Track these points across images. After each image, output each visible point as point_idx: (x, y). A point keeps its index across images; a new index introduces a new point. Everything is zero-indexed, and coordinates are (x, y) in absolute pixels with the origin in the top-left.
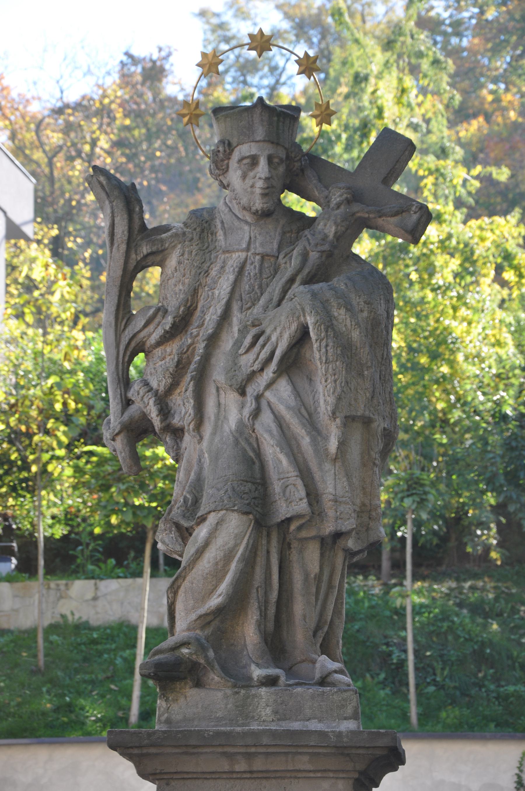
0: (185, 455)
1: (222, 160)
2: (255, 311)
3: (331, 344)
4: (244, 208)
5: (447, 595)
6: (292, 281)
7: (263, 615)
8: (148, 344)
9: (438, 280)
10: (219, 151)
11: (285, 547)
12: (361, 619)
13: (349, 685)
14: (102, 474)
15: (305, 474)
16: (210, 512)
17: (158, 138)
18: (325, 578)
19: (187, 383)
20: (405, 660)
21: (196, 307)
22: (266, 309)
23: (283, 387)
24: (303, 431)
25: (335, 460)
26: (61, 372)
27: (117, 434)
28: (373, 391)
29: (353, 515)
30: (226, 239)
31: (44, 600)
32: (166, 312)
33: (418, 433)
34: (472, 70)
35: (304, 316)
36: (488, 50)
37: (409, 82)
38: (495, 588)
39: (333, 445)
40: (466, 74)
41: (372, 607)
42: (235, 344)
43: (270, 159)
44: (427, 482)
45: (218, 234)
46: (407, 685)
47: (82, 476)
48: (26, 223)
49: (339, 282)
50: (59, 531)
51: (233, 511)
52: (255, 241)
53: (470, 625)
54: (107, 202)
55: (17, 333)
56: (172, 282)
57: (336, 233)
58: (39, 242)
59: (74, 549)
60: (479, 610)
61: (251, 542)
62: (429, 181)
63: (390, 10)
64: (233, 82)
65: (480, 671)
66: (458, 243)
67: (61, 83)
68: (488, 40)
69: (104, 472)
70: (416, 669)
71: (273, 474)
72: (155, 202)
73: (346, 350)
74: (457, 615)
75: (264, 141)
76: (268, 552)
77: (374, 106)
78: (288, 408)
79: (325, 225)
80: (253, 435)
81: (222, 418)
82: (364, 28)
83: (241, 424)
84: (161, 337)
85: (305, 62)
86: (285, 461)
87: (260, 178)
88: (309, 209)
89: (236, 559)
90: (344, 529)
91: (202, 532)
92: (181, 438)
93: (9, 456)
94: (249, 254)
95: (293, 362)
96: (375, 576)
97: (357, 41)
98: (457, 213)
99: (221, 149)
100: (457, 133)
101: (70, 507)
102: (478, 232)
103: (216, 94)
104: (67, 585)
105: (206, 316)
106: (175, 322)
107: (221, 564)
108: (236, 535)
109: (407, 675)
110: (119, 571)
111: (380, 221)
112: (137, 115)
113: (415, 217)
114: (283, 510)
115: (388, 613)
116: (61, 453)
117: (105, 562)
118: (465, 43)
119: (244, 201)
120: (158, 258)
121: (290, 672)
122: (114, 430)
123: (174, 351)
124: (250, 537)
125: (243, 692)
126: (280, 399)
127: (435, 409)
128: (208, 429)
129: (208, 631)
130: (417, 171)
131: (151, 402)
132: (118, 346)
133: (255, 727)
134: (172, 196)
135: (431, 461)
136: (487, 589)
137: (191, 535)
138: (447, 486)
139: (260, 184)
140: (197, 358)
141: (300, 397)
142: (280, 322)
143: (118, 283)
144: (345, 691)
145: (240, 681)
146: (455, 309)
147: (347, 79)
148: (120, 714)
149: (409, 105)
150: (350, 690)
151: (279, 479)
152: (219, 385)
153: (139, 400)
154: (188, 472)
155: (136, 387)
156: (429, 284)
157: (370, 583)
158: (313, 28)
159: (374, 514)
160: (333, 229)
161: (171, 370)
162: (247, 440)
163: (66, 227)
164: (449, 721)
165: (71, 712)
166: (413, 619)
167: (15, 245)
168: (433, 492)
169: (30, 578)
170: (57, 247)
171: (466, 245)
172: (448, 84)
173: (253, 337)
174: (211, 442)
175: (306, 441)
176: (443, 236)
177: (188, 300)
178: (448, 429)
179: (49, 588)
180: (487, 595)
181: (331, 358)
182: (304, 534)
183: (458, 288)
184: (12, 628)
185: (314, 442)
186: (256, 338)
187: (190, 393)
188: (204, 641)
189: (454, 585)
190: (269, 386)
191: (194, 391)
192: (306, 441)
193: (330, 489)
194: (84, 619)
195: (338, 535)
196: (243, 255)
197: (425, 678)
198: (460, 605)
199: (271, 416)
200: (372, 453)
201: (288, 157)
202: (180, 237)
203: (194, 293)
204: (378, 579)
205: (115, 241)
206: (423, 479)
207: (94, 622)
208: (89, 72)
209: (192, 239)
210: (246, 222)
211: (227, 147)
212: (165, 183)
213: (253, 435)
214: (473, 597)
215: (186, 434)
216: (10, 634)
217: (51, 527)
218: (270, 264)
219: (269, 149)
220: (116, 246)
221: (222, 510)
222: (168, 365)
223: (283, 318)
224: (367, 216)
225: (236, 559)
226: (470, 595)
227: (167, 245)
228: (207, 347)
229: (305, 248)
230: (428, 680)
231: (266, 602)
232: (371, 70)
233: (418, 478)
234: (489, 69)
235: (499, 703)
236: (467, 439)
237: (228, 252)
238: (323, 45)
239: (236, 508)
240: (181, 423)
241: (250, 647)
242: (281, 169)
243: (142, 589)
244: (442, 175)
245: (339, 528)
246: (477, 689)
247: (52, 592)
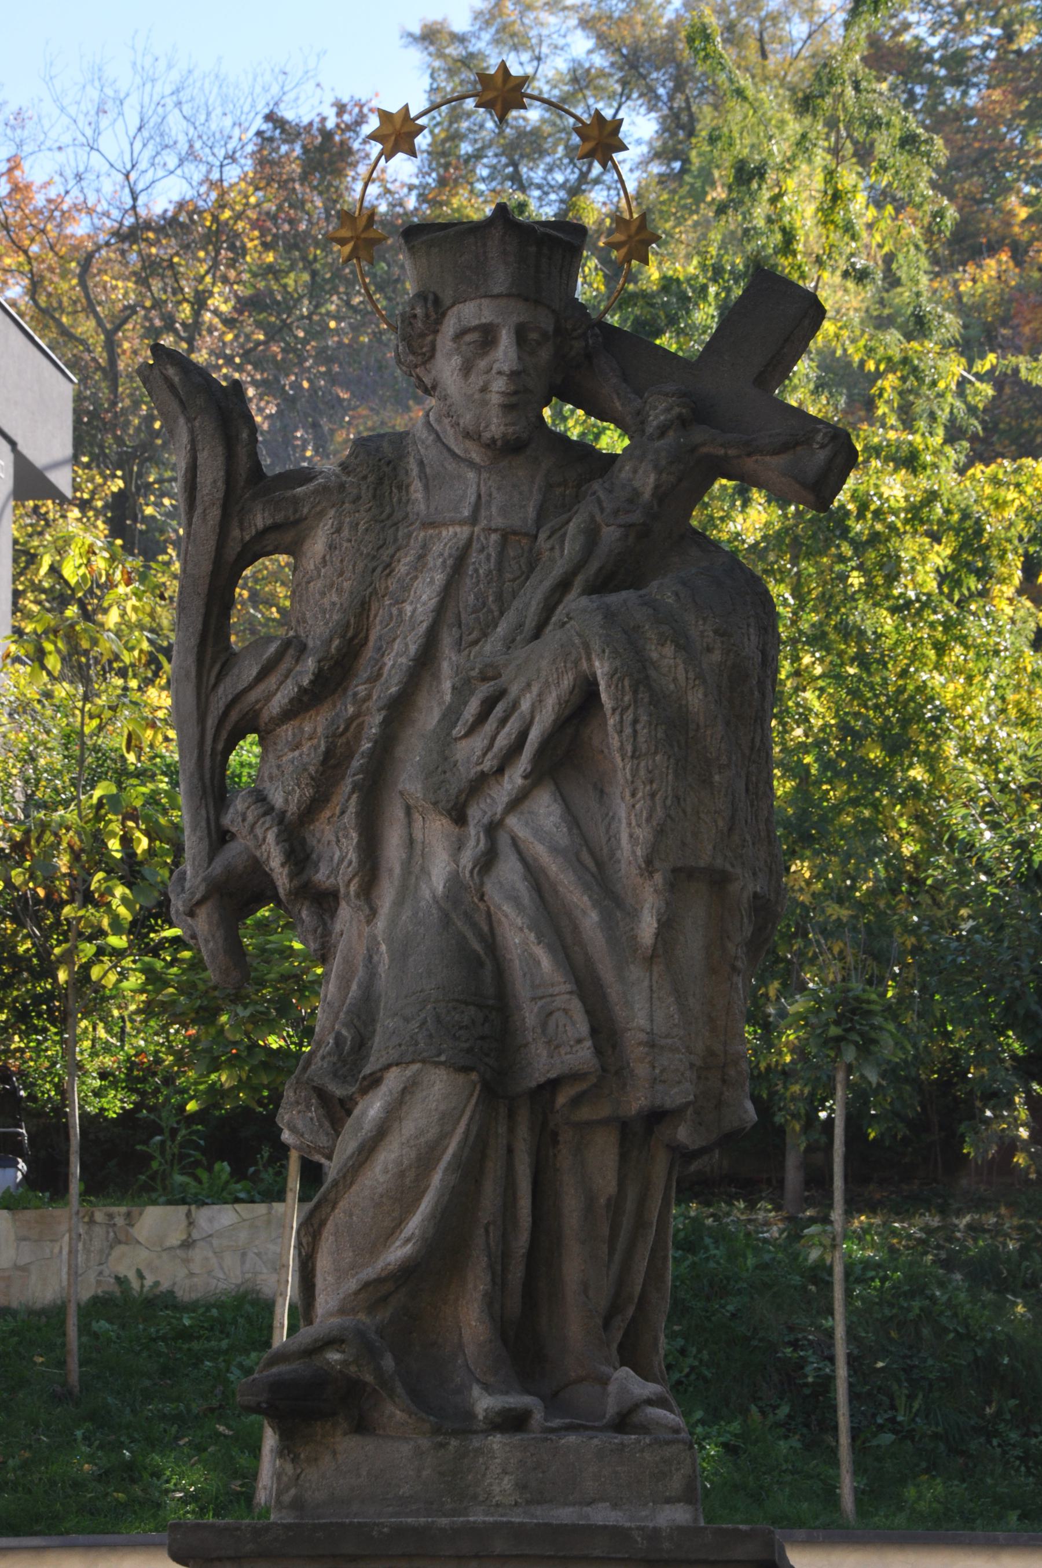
0: (340, 947)
1: (422, 335)
2: (488, 648)
3: (644, 718)
4: (467, 435)
5: (921, 1242)
6: (563, 586)
8: (265, 716)
9: (905, 588)
10: (415, 316)
11: (545, 1140)
12: (739, 1292)
13: (677, 1431)
14: (202, 987)
15: (588, 988)
16: (388, 1067)
17: (334, 290)
18: (630, 1205)
19: (345, 799)
20: (831, 1378)
21: (366, 638)
22: (510, 643)
23: (546, 808)
24: (585, 898)
25: (650, 960)
26: (122, 775)
27: (199, 903)
28: (733, 817)
29: (688, 1074)
30: (427, 499)
31: (80, 1246)
32: (303, 648)
33: (861, 907)
34: (986, 154)
35: (589, 659)
36: (1021, 115)
37: (848, 177)
38: (1022, 1229)
39: (647, 927)
40: (975, 163)
41: (764, 1267)
42: (444, 717)
43: (521, 335)
44: (877, 1008)
45: (412, 488)
46: (835, 1428)
47: (158, 992)
48: (56, 465)
49: (664, 590)
50: (115, 1104)
52: (489, 503)
53: (968, 1306)
54: (182, 421)
55: (32, 693)
56: (316, 586)
57: (657, 487)
58: (84, 505)
59: (146, 1142)
60: (990, 1275)
61: (474, 1129)
62: (890, 382)
63: (817, 31)
64: (491, 178)
65: (989, 1403)
66: (948, 512)
67: (133, 176)
68: (1021, 94)
69: (205, 981)
70: (854, 1396)
71: (521, 989)
72: (325, 424)
73: (675, 730)
74: (942, 1285)
75: (509, 296)
76: (510, 1151)
77: (776, 228)
79: (635, 472)
80: (481, 905)
81: (416, 869)
82: (764, 67)
83: (454, 881)
84: (291, 701)
85: (595, 133)
86: (546, 963)
87: (499, 373)
88: (612, 441)
89: (443, 1164)
90: (669, 1104)
91: (372, 1108)
92: (333, 913)
93: (15, 947)
95: (564, 755)
96: (771, 1201)
97: (740, 93)
98: (948, 450)
99: (419, 311)
100: (956, 284)
101: (140, 1052)
102: (988, 490)
103: (455, 202)
104: (128, 1215)
105: (386, 659)
107: (411, 1175)
108: (443, 1116)
109: (834, 1409)
110: (239, 1188)
111: (750, 464)
112: (294, 244)
113: (822, 456)
114: (542, 1063)
115: (796, 1280)
116: (118, 941)
117: (210, 1169)
118: (973, 98)
119: (467, 419)
120: (289, 537)
121: (553, 1402)
122: (193, 894)
123: (319, 730)
124: (471, 1118)
125: (454, 1443)
126: (538, 832)
127: (898, 855)
128: (387, 894)
129: (383, 1315)
130: (862, 363)
131: (271, 837)
132: (202, 720)
133: (478, 1517)
134: (363, 411)
135: (889, 965)
136: (1004, 1231)
137: (349, 1113)
138: (920, 1015)
139: (499, 385)
140: (366, 746)
141: (579, 827)
142: (539, 670)
143: (203, 588)
144: (668, 1443)
145: (450, 1421)
146: (941, 649)
147: (722, 174)
148: (236, 1486)
149: (848, 228)
150: (678, 1441)
151: (533, 999)
152: (411, 802)
153: (245, 832)
154: (345, 982)
155: (239, 804)
156: (887, 597)
157: (761, 1216)
158: (658, 69)
159: (732, 1072)
160: (652, 479)
161: (312, 769)
162: (468, 917)
163: (140, 475)
164: (922, 1506)
165: (133, 1481)
166: (848, 1293)
167: (36, 508)
168: (891, 1027)
169: (52, 1199)
170: (121, 516)
171: (966, 515)
172: (933, 184)
173: (483, 702)
174: (393, 922)
175: (590, 920)
176: (917, 498)
177: (348, 625)
178: (925, 899)
179: (92, 1222)
180: (1005, 1245)
181: (644, 748)
182: (585, 1113)
183: (947, 605)
184: (14, 1305)
185: (608, 922)
187: (350, 818)
188: (373, 1336)
189: (935, 1222)
190: (515, 804)
191: (358, 814)
192: (590, 920)
193: (641, 1020)
194: (165, 1286)
195: (656, 1117)
196: (463, 532)
197: (874, 1416)
198: (948, 1264)
199: (519, 866)
200: (730, 945)
201: (558, 331)
202: (333, 492)
203: (362, 609)
204: (778, 1208)
205: (198, 502)
206: (869, 1002)
207: (184, 1294)
208: (191, 155)
209: (359, 498)
210: (471, 464)
211: (433, 305)
212: (346, 386)
213: (481, 905)
214: (977, 1246)
215: (343, 904)
216: (9, 1318)
217: (98, 1093)
218: (519, 550)
219: (518, 313)
221: (413, 1062)
222: (305, 759)
223: (544, 663)
224: (722, 452)
225: (443, 1164)
226: (970, 1243)
227: (306, 510)
228: (386, 723)
229: (592, 518)
230: (880, 1421)
231: (506, 1255)
232: (771, 153)
233: (857, 999)
234: (1023, 154)
235: (1028, 1468)
236: (963, 919)
237: (432, 525)
238: (679, 102)
239: (443, 1058)
240: (332, 880)
241: (470, 1350)
242: (545, 354)
243: (283, 1224)
244: (915, 370)
245: (658, 1103)
246: (982, 1440)
247: (99, 1231)
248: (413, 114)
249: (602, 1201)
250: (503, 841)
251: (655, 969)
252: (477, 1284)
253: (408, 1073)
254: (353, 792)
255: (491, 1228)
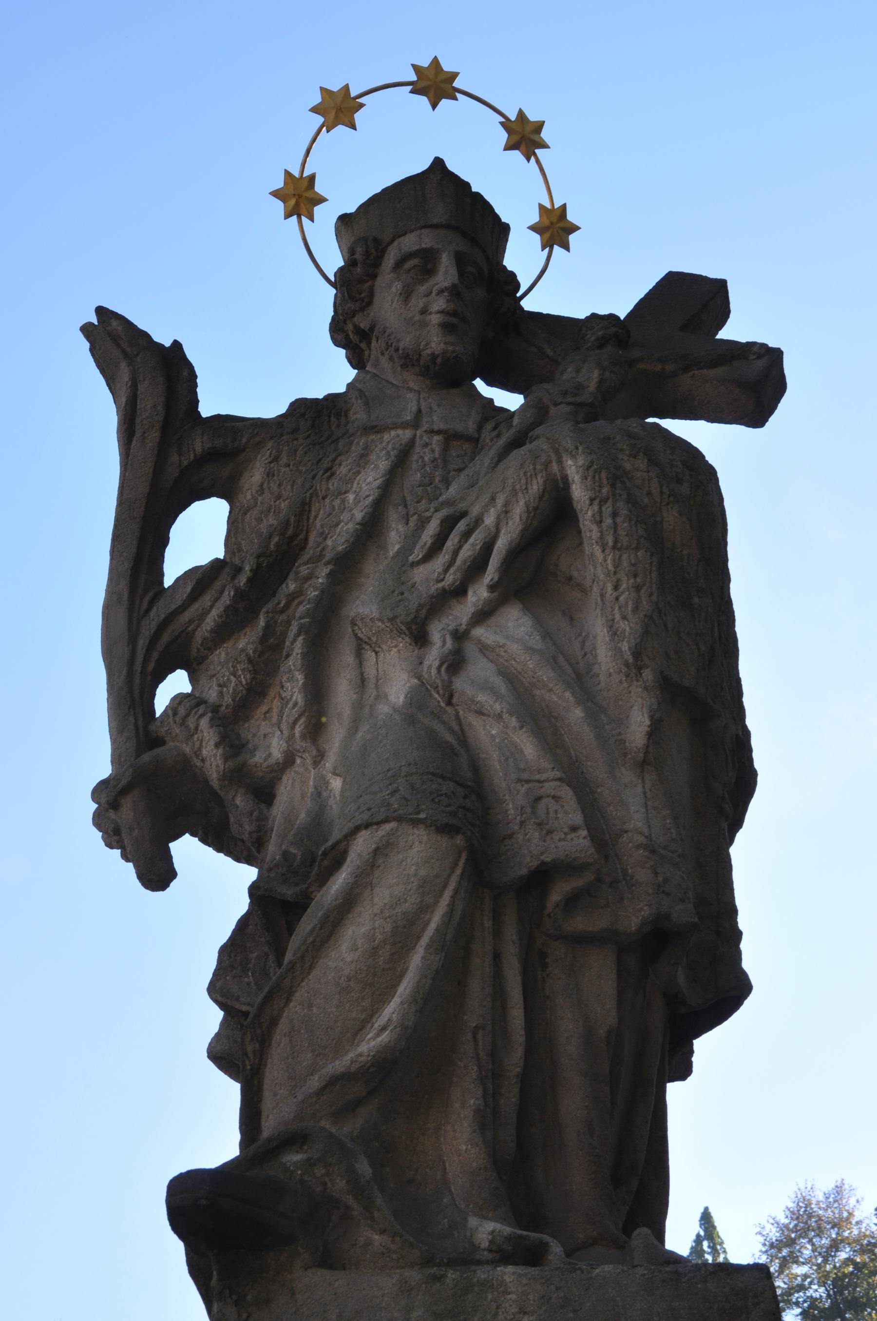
1: (361, 281)
7: (492, 1077)
16: (357, 830)
21: (306, 539)
23: (515, 627)
25: (642, 765)
35: (560, 461)
51: (415, 822)
71: (499, 774)
75: (447, 227)
76: (497, 956)
78: (532, 650)
83: (418, 699)
86: (529, 748)
89: (424, 941)
94: (418, 433)
106: (259, 566)
114: (530, 848)
124: (456, 891)
125: (452, 1275)
132: (132, 641)
139: (440, 304)
142: (504, 481)
160: (596, 373)
173: (443, 521)
177: (288, 523)
181: (625, 541)
182: (580, 923)
186: (449, 524)
190: (482, 616)
191: (304, 655)
196: (407, 434)
213: (449, 709)
220: (138, 434)
224: (659, 367)
225: (424, 941)
227: (244, 440)
248: (353, 94)
249: (602, 1032)
250: (470, 649)
251: (647, 777)
252: (465, 1100)
253: (381, 833)
254: (298, 634)
255: (480, 1035)
